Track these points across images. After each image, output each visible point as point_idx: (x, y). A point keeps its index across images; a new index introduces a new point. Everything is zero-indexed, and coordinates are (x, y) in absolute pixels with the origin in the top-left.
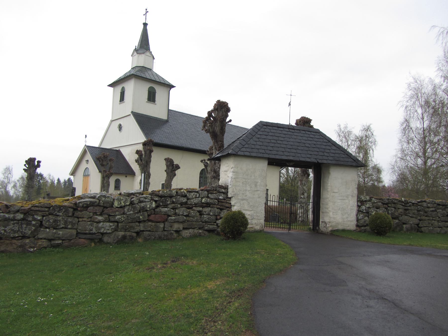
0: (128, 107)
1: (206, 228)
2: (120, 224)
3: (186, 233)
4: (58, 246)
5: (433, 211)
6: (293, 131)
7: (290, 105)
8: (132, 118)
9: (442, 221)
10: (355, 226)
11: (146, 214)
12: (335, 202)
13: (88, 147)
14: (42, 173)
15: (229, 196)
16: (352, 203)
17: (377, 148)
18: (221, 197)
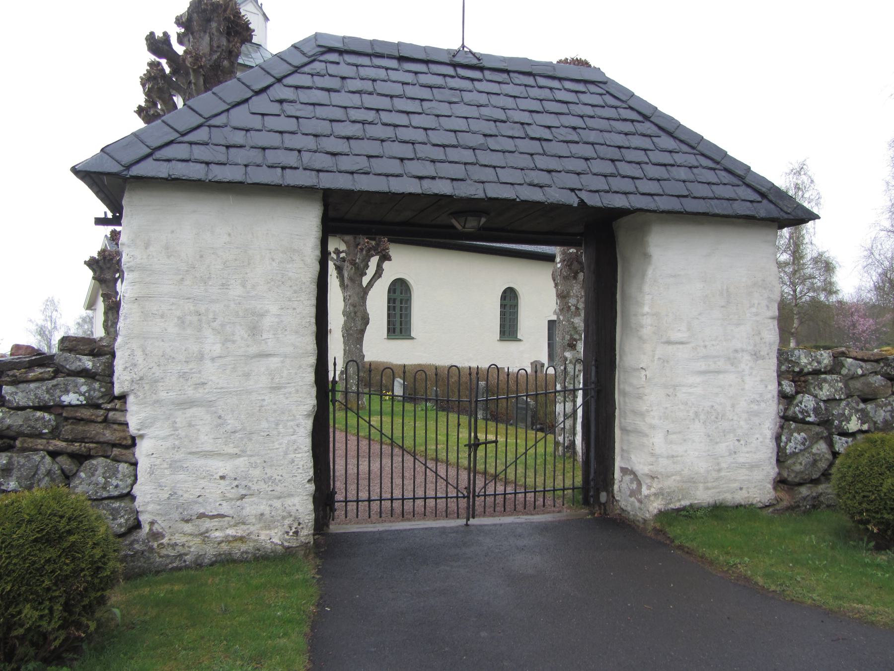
6: (477, 74)
12: (675, 387)
15: (117, 391)
16: (754, 391)
18: (71, 398)
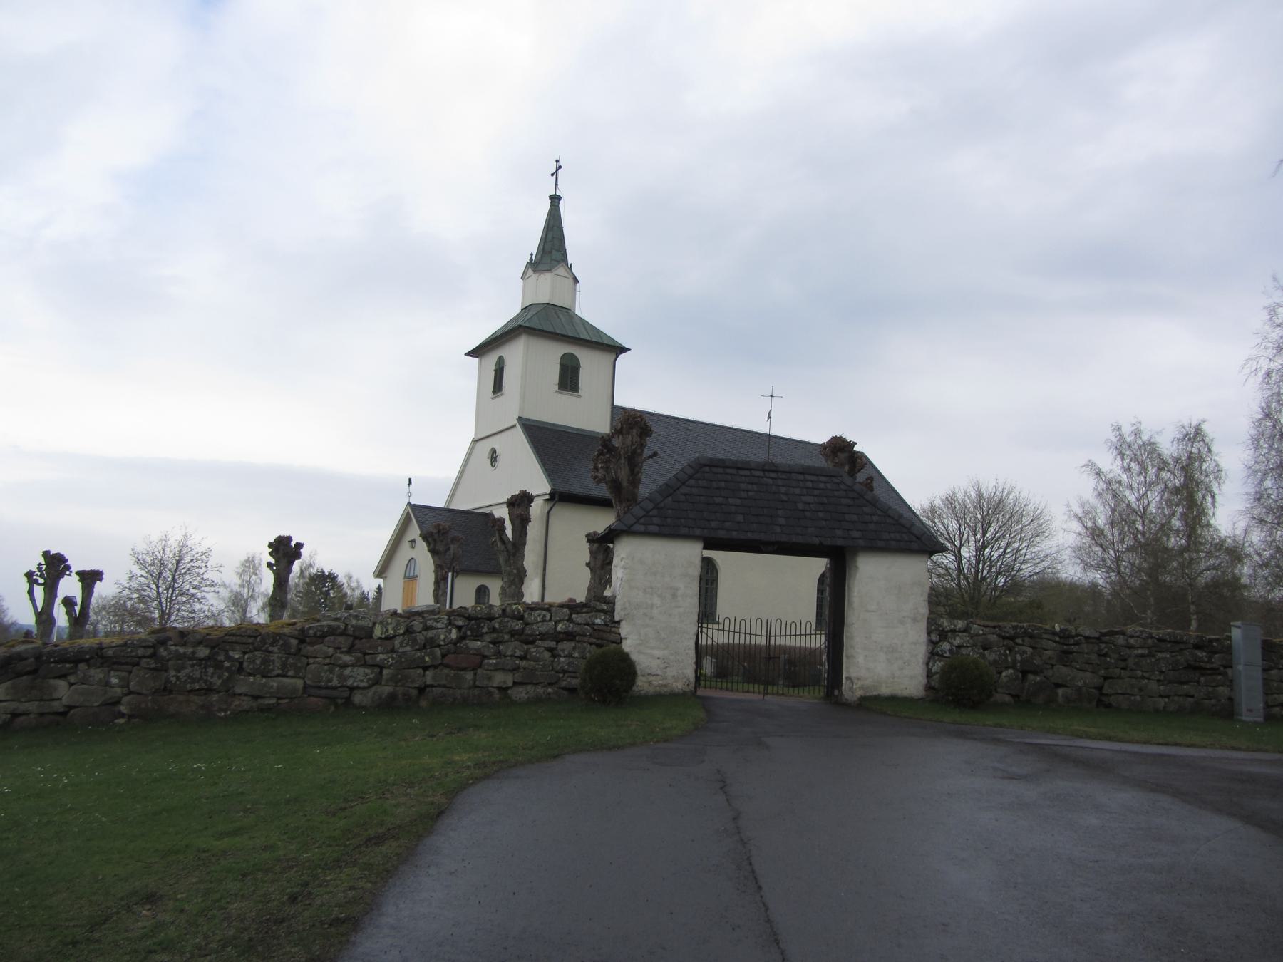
0: (510, 408)
1: (564, 684)
2: (385, 672)
3: (520, 694)
4: (269, 709)
5: (1142, 656)
7: (770, 417)
8: (519, 431)
9: (1170, 682)
10: (921, 688)
11: (438, 652)
13: (414, 508)
14: (335, 572)
15: (617, 619)
16: (914, 640)
17: (1224, 488)
18: (598, 621)
